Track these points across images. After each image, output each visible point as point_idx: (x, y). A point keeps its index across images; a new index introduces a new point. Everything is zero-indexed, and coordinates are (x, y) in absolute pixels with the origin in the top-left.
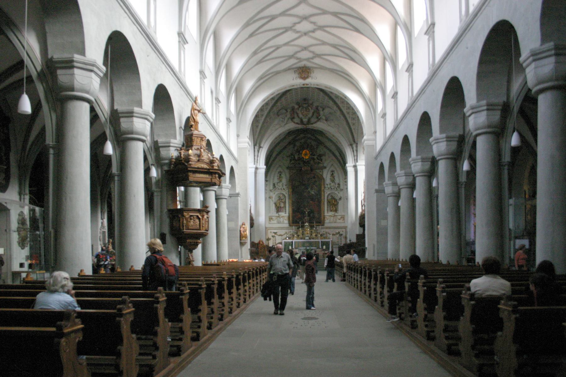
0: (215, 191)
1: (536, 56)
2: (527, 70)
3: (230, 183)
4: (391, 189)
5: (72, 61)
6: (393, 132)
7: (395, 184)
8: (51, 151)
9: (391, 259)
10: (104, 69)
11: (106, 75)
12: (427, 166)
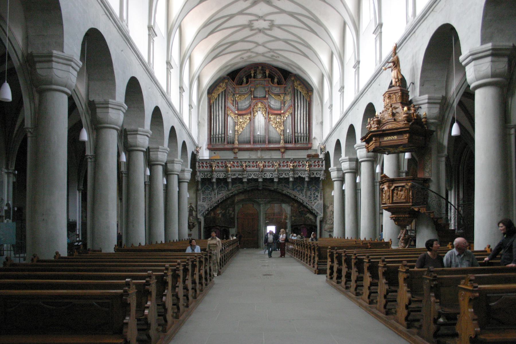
0: (178, 175)
1: (476, 57)
2: (467, 68)
3: (182, 158)
4: (348, 164)
5: (137, 131)
6: (352, 106)
7: (339, 170)
8: (124, 175)
9: (339, 238)
10: (81, 64)
11: (81, 69)
12: (354, 164)
